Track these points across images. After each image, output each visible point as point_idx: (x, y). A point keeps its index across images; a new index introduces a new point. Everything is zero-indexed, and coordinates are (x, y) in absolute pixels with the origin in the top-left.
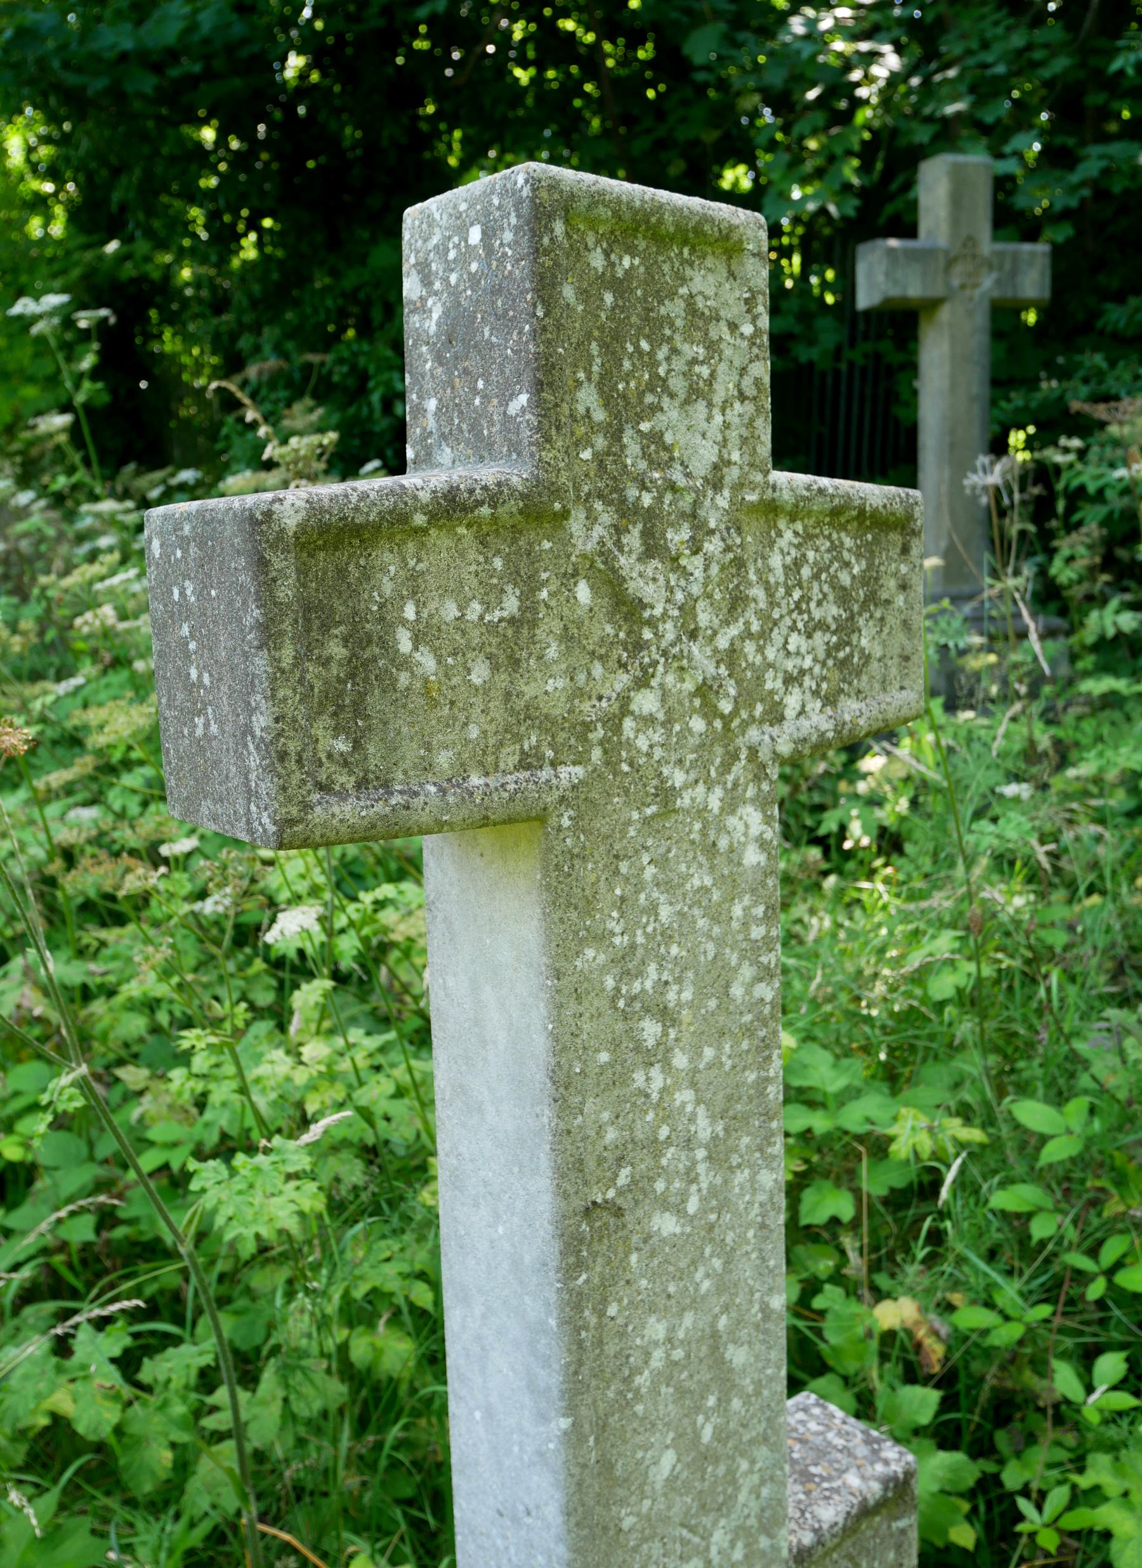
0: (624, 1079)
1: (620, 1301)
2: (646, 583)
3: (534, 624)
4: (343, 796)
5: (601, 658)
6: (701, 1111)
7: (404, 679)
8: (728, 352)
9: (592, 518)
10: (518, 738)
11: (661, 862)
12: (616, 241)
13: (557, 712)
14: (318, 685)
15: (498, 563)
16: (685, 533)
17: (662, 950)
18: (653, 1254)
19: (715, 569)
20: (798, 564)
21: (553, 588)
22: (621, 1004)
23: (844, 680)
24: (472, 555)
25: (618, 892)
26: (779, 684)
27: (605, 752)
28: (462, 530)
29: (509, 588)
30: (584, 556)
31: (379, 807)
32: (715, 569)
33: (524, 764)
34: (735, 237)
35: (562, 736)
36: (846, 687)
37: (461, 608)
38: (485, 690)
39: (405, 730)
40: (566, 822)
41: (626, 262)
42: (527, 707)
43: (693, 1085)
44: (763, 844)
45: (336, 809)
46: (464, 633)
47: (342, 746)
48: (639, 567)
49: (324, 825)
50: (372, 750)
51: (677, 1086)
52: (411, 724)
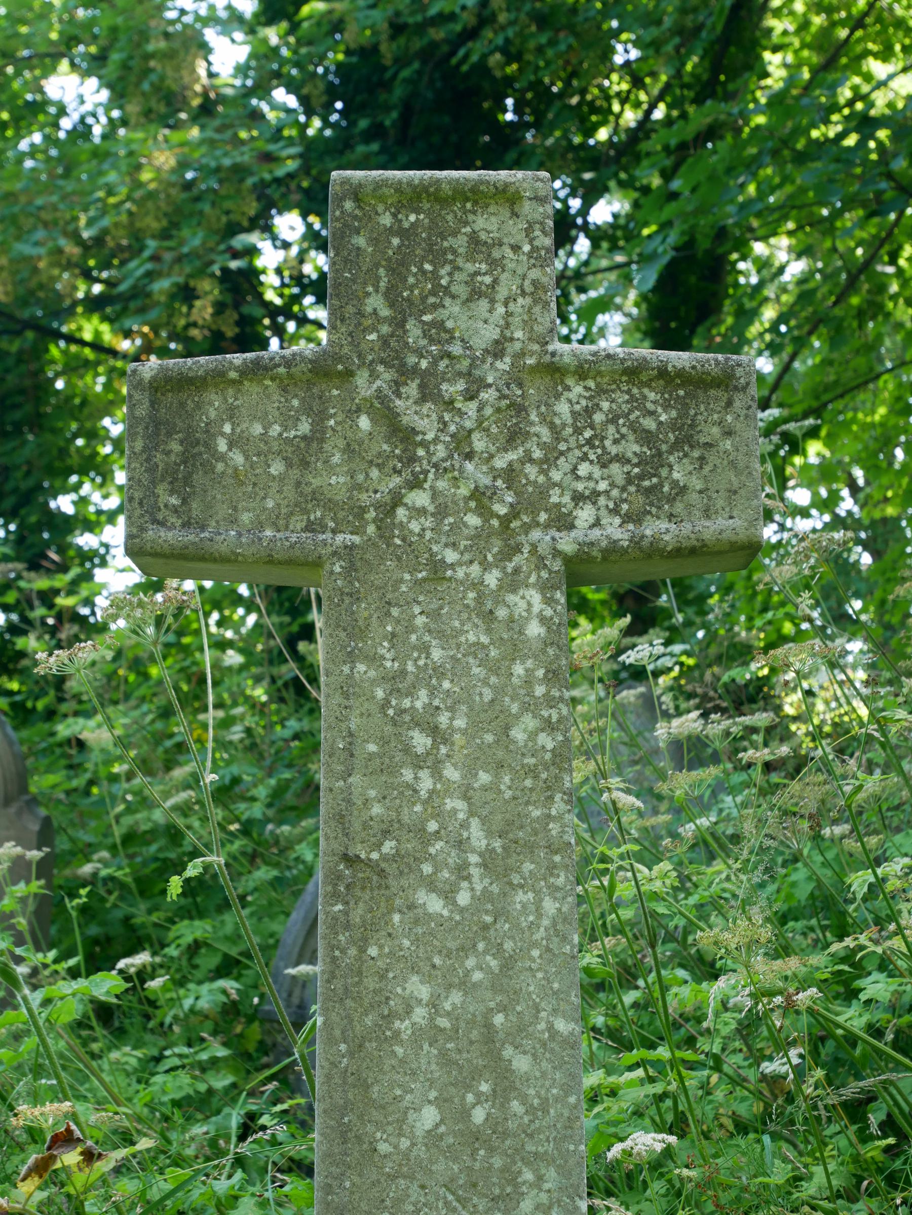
0: (393, 770)
1: (381, 947)
2: (424, 421)
3: (322, 440)
4: (172, 527)
5: (378, 465)
6: (475, 823)
7: (220, 467)
8: (510, 265)
9: (374, 376)
10: (306, 512)
11: (434, 615)
12: (403, 206)
13: (338, 498)
14: (161, 466)
15: (296, 403)
16: (461, 385)
17: (434, 681)
18: (416, 922)
19: (488, 411)
20: (588, 412)
21: (339, 419)
22: (391, 712)
23: (651, 504)
24: (275, 397)
25: (389, 628)
26: (566, 499)
27: (379, 528)
28: (268, 382)
29: (304, 418)
30: (365, 399)
31: (191, 537)
32: (488, 411)
33: (310, 527)
34: (512, 189)
35: (341, 515)
36: (654, 510)
37: (264, 428)
38: (281, 478)
39: (219, 496)
40: (337, 569)
41: (412, 218)
42: (314, 493)
43: (466, 797)
44: (543, 620)
45: (162, 534)
46: (266, 443)
47: (174, 501)
48: (414, 408)
49: (153, 541)
50: (194, 506)
51: (448, 793)
52: (224, 494)
